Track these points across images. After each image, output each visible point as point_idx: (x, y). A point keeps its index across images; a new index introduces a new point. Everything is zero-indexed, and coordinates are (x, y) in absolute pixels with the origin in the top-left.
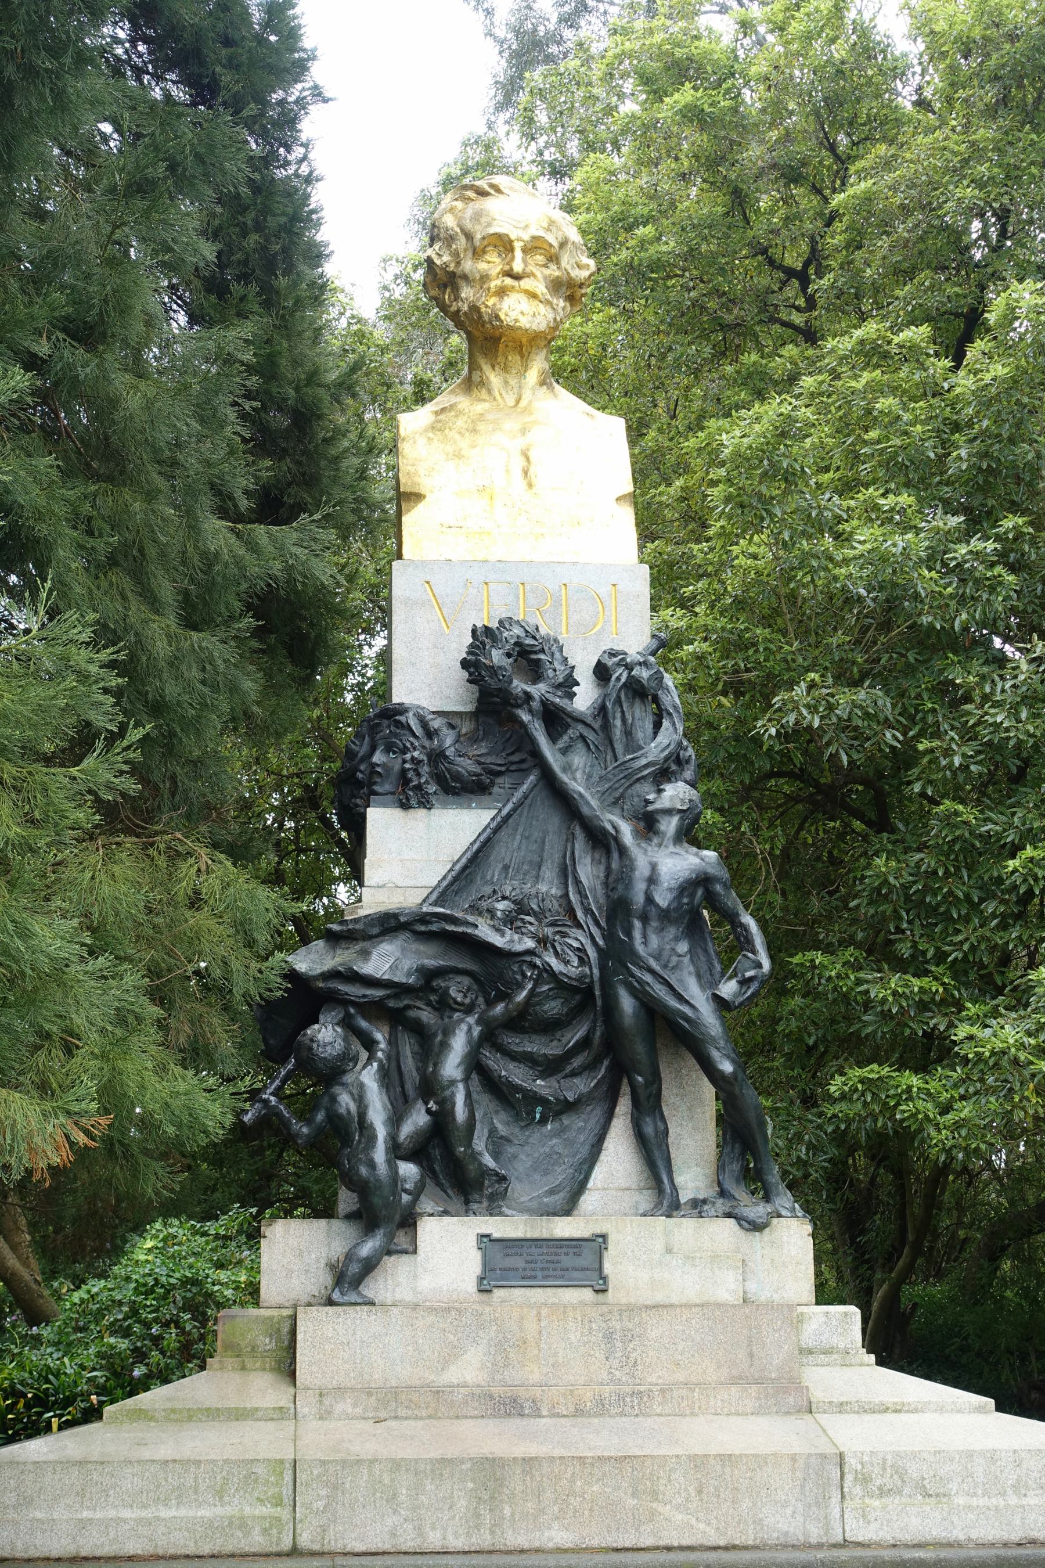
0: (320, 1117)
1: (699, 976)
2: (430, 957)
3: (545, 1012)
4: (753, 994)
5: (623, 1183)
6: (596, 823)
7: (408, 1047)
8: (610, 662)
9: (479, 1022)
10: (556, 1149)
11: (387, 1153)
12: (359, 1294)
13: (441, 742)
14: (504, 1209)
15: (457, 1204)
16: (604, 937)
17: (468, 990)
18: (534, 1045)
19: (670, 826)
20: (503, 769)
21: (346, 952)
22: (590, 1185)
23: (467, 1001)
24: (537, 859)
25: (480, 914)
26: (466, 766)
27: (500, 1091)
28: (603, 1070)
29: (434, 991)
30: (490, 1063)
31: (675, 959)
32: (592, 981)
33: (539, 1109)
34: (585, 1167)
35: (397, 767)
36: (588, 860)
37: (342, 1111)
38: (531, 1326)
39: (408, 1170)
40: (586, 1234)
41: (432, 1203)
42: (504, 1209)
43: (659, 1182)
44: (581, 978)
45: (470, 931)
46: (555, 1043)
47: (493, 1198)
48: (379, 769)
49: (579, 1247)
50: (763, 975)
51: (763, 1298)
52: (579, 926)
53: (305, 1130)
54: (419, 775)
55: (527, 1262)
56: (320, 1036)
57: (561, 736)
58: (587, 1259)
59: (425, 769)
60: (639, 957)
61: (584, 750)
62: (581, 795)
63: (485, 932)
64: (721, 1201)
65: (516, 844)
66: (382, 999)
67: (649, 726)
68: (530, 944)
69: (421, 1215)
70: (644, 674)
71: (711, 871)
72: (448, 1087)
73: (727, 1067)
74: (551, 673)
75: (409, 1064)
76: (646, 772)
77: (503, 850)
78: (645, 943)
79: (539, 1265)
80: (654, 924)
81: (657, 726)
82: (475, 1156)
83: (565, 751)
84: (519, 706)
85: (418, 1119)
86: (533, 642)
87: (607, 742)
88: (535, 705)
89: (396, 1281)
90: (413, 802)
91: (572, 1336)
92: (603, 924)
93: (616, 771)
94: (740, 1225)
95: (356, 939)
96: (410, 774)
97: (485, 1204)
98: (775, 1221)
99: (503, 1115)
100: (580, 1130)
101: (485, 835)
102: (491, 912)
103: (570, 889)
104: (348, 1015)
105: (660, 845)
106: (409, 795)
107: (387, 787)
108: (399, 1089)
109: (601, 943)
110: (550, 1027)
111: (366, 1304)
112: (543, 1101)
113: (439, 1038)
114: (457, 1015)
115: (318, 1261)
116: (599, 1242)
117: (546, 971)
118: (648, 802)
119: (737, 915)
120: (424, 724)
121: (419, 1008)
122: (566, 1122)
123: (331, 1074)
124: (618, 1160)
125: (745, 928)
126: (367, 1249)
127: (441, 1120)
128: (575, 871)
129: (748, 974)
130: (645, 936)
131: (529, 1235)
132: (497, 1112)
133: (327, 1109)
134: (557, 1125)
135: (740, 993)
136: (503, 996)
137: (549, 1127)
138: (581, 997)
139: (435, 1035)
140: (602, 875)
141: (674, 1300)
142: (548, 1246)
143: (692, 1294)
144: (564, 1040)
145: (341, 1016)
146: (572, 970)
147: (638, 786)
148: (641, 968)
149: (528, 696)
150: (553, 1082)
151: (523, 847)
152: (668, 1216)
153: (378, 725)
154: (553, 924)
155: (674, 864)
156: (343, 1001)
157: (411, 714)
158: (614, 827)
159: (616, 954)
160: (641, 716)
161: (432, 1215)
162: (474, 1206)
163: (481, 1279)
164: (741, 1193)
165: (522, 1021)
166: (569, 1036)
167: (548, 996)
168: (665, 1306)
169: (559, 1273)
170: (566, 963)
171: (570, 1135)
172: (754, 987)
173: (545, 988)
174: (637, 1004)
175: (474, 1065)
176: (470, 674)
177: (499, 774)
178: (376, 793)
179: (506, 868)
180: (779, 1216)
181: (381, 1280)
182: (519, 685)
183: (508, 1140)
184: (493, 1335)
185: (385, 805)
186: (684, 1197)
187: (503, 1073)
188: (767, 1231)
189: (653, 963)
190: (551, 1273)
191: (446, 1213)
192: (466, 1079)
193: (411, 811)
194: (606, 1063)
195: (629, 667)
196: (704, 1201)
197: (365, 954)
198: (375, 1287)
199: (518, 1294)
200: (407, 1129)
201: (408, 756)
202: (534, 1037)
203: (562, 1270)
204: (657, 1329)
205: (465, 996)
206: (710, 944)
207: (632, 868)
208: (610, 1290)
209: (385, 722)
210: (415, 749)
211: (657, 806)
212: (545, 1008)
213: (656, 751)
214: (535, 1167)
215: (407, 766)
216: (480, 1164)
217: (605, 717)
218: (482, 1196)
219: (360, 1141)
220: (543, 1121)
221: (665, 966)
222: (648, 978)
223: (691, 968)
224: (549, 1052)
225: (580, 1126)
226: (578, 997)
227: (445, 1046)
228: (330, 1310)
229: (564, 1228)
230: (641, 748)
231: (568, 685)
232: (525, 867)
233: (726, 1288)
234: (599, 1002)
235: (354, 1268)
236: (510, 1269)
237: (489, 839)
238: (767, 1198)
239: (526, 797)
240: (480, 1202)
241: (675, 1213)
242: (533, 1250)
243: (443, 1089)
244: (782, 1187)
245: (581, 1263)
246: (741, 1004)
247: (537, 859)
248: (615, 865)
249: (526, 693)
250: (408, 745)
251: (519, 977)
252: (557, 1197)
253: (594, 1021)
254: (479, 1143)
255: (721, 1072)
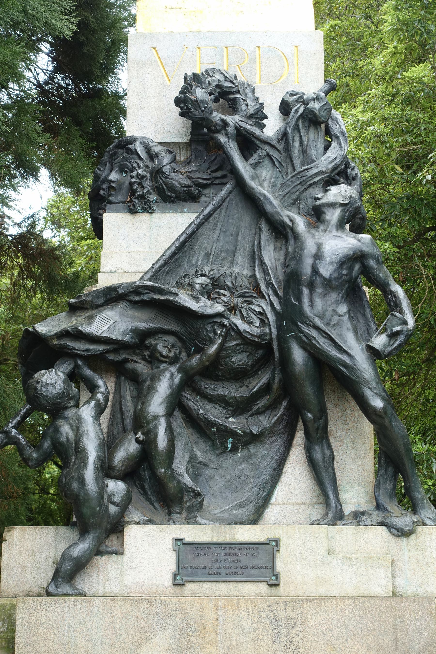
0: (47, 444)
1: (356, 332)
2: (142, 321)
3: (233, 363)
4: (399, 345)
5: (300, 499)
6: (277, 217)
7: (128, 393)
8: (291, 99)
9: (179, 371)
10: (244, 472)
11: (95, 472)
12: (75, 588)
13: (161, 162)
14: (199, 519)
15: (162, 514)
16: (280, 302)
17: (173, 346)
18: (228, 390)
19: (333, 216)
20: (208, 182)
21: (79, 318)
22: (273, 500)
23: (172, 354)
24: (232, 248)
25: (183, 288)
26: (179, 180)
27: (195, 423)
28: (282, 410)
29: (147, 348)
30: (191, 404)
31: (336, 318)
32: (271, 338)
33: (230, 440)
34: (268, 486)
35: (127, 183)
36: (272, 247)
37: (63, 439)
38: (210, 615)
39: (116, 487)
40: (262, 539)
41: (139, 514)
42: (199, 519)
43: (326, 497)
44: (262, 336)
45: (171, 298)
46: (244, 388)
47: (190, 510)
48: (113, 185)
49: (256, 549)
50: (408, 330)
51: (410, 592)
52: (262, 296)
53: (35, 455)
54: (143, 187)
55: (213, 561)
56: (44, 379)
57: (252, 155)
58: (262, 559)
59: (147, 184)
60: (307, 317)
61: (270, 166)
62: (264, 196)
63: (185, 299)
64: (377, 513)
65: (216, 236)
66: (102, 354)
67: (321, 146)
68: (219, 308)
69: (129, 523)
70: (316, 106)
71: (366, 249)
72: (152, 421)
73: (378, 403)
74: (244, 107)
75: (129, 406)
76: (317, 179)
77: (205, 241)
78: (312, 306)
79: (223, 564)
80: (319, 290)
81: (327, 148)
82: (173, 475)
83: (255, 166)
84: (218, 132)
85: (129, 448)
86: (230, 85)
87: (288, 160)
88: (231, 129)
89: (107, 576)
90: (138, 208)
91: (244, 624)
92: (280, 293)
93: (294, 179)
94: (391, 532)
95: (87, 309)
96: (135, 187)
97: (184, 515)
98: (419, 529)
99: (203, 446)
100: (264, 457)
101: (190, 229)
102: (191, 285)
103: (257, 269)
104: (77, 366)
105: (325, 231)
106: (137, 204)
107: (120, 198)
108: (120, 425)
109: (278, 307)
110: (239, 375)
111: (76, 595)
112: (233, 434)
113: (148, 383)
114: (163, 366)
115: (47, 559)
116: (272, 546)
117: (234, 330)
118: (317, 199)
119: (388, 284)
120: (148, 149)
121: (135, 362)
122: (252, 451)
123: (57, 408)
124: (295, 480)
125: (394, 295)
126: (77, 551)
127: (147, 446)
128: (260, 256)
129: (395, 329)
130: (311, 300)
131: (215, 540)
132: (197, 443)
133: (52, 439)
134: (245, 453)
135: (389, 345)
136: (200, 350)
137: (239, 455)
138: (265, 352)
139: (145, 381)
140: (282, 258)
141: (335, 593)
142: (230, 549)
143: (349, 589)
144: (251, 386)
145: (72, 366)
146: (254, 329)
147: (311, 190)
148: (308, 325)
149: (225, 124)
150: (243, 419)
151: (222, 239)
152: (330, 525)
153: (115, 153)
154: (242, 296)
155: (337, 244)
156: (72, 355)
157: (138, 143)
158: (291, 221)
159: (290, 316)
160: (314, 139)
161: (138, 523)
162: (175, 516)
163: (176, 575)
164: (393, 507)
165: (214, 370)
166: (255, 383)
167: (235, 350)
168: (327, 598)
169: (240, 570)
170: (251, 324)
171: (256, 460)
172: (400, 339)
173: (233, 343)
174: (306, 355)
175: (176, 404)
176: (181, 109)
177: (205, 186)
178: (110, 203)
179: (208, 255)
180: (424, 525)
181: (94, 576)
182: (217, 116)
183: (206, 465)
184: (178, 622)
185: (117, 211)
186: (347, 510)
187: (201, 411)
188: (413, 536)
189: (318, 322)
190: (233, 570)
191: (150, 521)
192: (169, 414)
193: (138, 215)
194: (284, 404)
195: (305, 103)
196: (363, 513)
197: (91, 318)
198: (85, 583)
199: (206, 588)
200: (120, 456)
201: (135, 173)
202: (226, 383)
203: (242, 568)
204: (316, 617)
205: (170, 351)
206: (368, 310)
207: (302, 248)
208: (282, 585)
209: (120, 151)
210: (139, 168)
211: (324, 201)
212: (234, 359)
213: (325, 163)
214: (227, 486)
215: (133, 180)
216: (179, 482)
217: (287, 141)
218: (181, 508)
219: (75, 463)
220: (235, 449)
221: (328, 324)
222: (314, 333)
223: (349, 326)
224: (237, 395)
225: (264, 454)
226: (261, 352)
227: (152, 389)
228: (45, 600)
229: (245, 533)
230: (313, 161)
231: (259, 117)
232: (223, 254)
233: (378, 583)
234: (277, 354)
235: (68, 566)
236: (199, 567)
237: (193, 233)
238: (415, 511)
239: (223, 201)
240: (180, 513)
241: (338, 523)
242: (218, 551)
243: (148, 423)
244: (426, 502)
245: (256, 563)
246: (390, 353)
247: (232, 248)
248: (290, 250)
249: (223, 121)
250: (135, 165)
251: (211, 335)
252: (244, 510)
253: (274, 371)
254: (180, 465)
255: (374, 409)
